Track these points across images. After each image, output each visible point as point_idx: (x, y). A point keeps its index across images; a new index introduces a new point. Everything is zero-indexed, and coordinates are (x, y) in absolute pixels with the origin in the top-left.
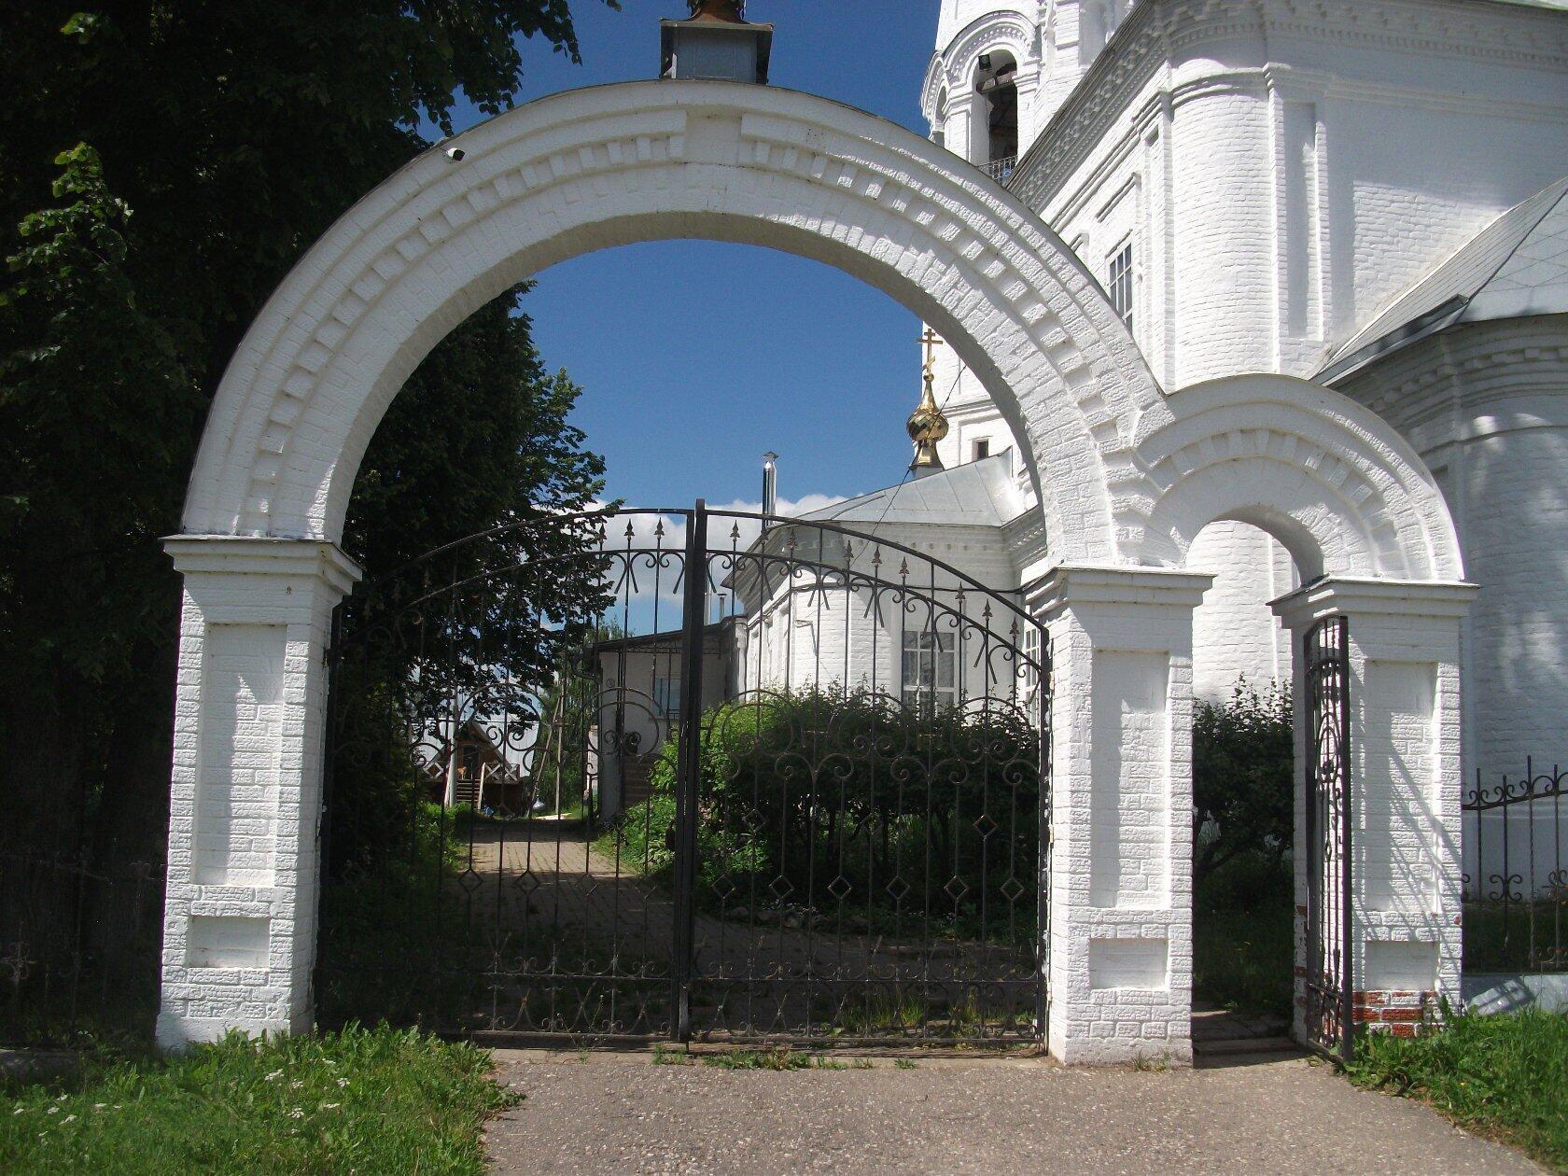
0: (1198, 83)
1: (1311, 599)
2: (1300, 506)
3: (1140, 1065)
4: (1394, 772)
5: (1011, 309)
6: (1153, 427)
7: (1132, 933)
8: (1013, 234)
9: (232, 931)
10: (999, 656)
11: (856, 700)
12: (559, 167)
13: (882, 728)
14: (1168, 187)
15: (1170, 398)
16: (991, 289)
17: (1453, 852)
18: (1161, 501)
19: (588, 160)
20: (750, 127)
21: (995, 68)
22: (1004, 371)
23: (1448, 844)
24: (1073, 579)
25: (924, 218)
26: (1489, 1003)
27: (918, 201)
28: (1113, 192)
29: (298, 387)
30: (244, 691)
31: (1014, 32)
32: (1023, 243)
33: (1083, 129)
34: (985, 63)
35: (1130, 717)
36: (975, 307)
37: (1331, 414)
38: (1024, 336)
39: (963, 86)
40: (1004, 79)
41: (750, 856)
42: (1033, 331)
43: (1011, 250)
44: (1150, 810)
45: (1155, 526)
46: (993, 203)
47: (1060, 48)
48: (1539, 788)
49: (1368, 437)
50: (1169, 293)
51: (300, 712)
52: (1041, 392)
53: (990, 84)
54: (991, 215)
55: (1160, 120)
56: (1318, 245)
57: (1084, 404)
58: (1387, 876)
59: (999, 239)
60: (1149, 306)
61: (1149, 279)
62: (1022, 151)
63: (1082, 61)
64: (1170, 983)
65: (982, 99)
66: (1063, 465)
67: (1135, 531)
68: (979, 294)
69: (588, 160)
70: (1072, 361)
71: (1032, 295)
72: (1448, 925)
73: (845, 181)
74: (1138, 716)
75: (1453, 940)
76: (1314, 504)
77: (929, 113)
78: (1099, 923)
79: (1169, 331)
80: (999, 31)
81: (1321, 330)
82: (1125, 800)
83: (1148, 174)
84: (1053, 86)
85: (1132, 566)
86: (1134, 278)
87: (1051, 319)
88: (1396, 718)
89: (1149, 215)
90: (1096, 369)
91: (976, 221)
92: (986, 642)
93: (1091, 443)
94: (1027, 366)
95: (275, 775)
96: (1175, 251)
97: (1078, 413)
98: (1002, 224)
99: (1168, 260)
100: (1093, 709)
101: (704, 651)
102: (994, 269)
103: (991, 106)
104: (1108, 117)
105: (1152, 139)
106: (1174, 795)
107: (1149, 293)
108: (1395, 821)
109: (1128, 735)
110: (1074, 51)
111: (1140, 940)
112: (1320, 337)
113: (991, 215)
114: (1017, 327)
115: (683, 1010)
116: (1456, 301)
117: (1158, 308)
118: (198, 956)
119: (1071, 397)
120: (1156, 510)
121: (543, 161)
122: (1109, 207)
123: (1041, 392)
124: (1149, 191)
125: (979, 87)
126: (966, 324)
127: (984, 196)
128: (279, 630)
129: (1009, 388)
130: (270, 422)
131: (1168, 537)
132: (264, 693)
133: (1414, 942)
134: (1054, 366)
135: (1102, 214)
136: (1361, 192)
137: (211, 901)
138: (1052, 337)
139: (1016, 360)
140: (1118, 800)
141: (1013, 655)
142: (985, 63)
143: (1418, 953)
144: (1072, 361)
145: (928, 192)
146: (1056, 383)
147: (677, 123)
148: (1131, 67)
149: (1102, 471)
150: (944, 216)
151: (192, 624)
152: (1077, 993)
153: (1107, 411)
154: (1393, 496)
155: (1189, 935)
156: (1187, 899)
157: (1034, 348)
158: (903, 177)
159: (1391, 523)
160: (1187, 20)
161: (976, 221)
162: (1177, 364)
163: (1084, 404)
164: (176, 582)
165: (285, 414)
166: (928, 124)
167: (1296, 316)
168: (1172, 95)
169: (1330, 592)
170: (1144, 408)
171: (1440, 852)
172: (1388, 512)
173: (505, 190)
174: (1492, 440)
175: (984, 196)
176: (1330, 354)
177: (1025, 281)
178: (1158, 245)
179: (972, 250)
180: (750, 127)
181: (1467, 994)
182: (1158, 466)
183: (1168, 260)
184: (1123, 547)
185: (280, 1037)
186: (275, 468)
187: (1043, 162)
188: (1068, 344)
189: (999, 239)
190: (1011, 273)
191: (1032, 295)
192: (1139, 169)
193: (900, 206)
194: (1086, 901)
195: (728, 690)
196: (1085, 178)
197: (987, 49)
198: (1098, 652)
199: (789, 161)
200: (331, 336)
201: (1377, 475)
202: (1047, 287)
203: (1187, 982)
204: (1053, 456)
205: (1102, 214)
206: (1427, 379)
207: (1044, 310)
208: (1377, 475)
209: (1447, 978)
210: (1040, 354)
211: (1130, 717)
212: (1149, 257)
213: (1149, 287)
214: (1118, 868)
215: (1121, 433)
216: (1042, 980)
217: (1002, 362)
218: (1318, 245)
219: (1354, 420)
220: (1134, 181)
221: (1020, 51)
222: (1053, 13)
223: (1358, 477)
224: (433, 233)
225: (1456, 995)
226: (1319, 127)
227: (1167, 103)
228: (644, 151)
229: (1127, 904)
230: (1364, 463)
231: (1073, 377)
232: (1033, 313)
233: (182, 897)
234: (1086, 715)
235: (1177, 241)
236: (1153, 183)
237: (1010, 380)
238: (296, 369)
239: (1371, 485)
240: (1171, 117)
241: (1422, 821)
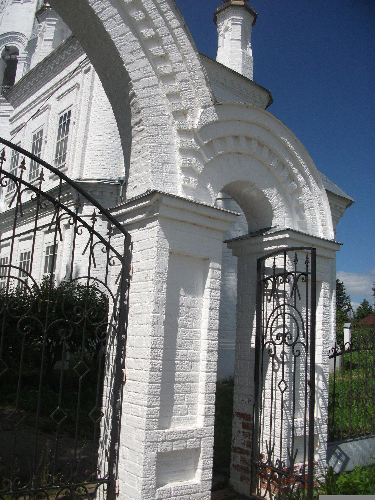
1: (265, 239)
2: (267, 187)
10: (99, 248)
17: (326, 384)
21: (11, 52)
22: (126, 62)
23: (324, 380)
24: (165, 201)
28: (66, 89)
31: (20, 41)
33: (55, 65)
34: (7, 49)
36: (112, 17)
37: (286, 140)
38: (138, 45)
40: (13, 57)
44: (192, 361)
47: (45, 40)
49: (299, 157)
50: (86, 131)
52: (145, 82)
53: (8, 57)
60: (76, 134)
61: (78, 124)
62: (15, 83)
65: (3, 62)
66: (154, 130)
68: (115, 11)
70: (166, 68)
71: (148, 21)
72: (323, 424)
74: (189, 298)
76: (272, 188)
78: (163, 441)
79: (85, 144)
80: (15, 39)
82: (180, 353)
83: (83, 84)
84: (41, 53)
86: (71, 123)
87: (157, 39)
89: (81, 99)
90: (180, 76)
92: (91, 239)
93: (171, 122)
96: (91, 114)
97: (165, 101)
99: (88, 117)
100: (167, 292)
104: (67, 63)
106: (209, 351)
107: (77, 129)
109: (183, 310)
110: (51, 43)
111: (186, 450)
114: (135, 39)
120: (204, 170)
122: (63, 95)
123: (145, 82)
124: (82, 90)
126: (106, 24)
129: (127, 73)
131: (206, 188)
134: (154, 69)
135: (59, 98)
138: (156, 50)
139: (133, 58)
140: (175, 355)
141: (108, 251)
142: (7, 49)
144: (166, 68)
146: (154, 79)
148: (75, 49)
149: (177, 141)
153: (182, 104)
154: (306, 190)
155: (212, 444)
156: (212, 420)
157: (143, 55)
159: (303, 205)
162: (86, 158)
163: (171, 96)
169: (286, 235)
170: (204, 107)
172: (302, 199)
177: (145, 11)
178: (83, 111)
182: (207, 144)
183: (88, 117)
184: (185, 188)
187: (35, 77)
191: (148, 21)
192: (80, 82)
194: (156, 426)
196: (53, 84)
197: (9, 44)
201: (300, 178)
203: (210, 475)
204: (150, 123)
207: (153, 33)
208: (300, 178)
210: (147, 60)
211: (185, 299)
212: (79, 116)
213: (77, 127)
214: (173, 400)
215: (189, 119)
219: (294, 147)
220: (77, 86)
221: (21, 48)
222: (45, 27)
223: (292, 178)
229: (177, 427)
230: (295, 171)
232: (148, 33)
235: (92, 110)
237: (128, 68)
239: (297, 183)
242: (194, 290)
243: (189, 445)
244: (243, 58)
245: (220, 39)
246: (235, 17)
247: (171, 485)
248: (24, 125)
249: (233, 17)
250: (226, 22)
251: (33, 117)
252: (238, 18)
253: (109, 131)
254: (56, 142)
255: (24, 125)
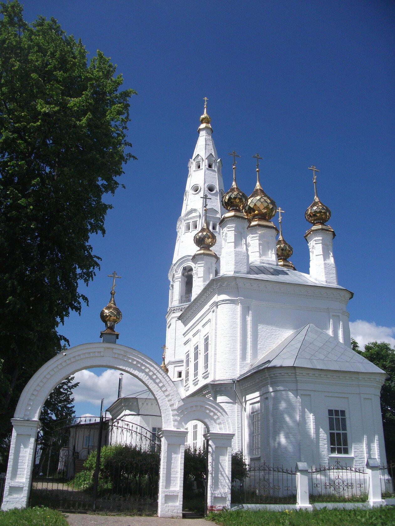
0: (223, 301)
3: (173, 518)
4: (220, 466)
5: (157, 384)
6: (180, 405)
7: (172, 494)
8: (158, 371)
9: (15, 489)
11: (135, 448)
12: (82, 357)
13: (142, 455)
14: (216, 324)
15: (183, 400)
16: (154, 380)
18: (181, 418)
19: (87, 355)
20: (114, 351)
21: (187, 270)
23: (229, 479)
25: (143, 368)
26: (235, 508)
27: (142, 365)
29: (35, 393)
30: (22, 446)
32: (159, 373)
34: (185, 269)
35: (174, 456)
39: (179, 274)
40: (190, 273)
41: (109, 486)
42: (161, 388)
43: (157, 374)
45: (180, 422)
46: (155, 366)
48: (252, 469)
51: (32, 451)
54: (154, 368)
55: (215, 308)
56: (249, 340)
57: (169, 401)
58: (218, 485)
59: (155, 372)
63: (204, 281)
64: (179, 503)
67: (176, 423)
69: (87, 355)
70: (167, 393)
71: (161, 381)
73: (130, 361)
75: (229, 497)
77: (170, 279)
81: (249, 360)
82: (172, 470)
85: (175, 429)
87: (164, 386)
88: (220, 457)
91: (152, 368)
94: (159, 394)
95: (27, 461)
98: (156, 369)
101: (103, 428)
102: (154, 377)
103: (186, 279)
105: (213, 311)
108: (220, 475)
110: (202, 279)
111: (173, 495)
112: (249, 362)
113: (154, 368)
115: (94, 506)
116: (269, 362)
117: (213, 353)
118: (10, 493)
119: (167, 399)
121: (79, 355)
125: (183, 274)
127: (153, 364)
128: (29, 436)
130: (30, 399)
132: (26, 446)
133: (222, 497)
136: (260, 327)
137: (14, 484)
138: (164, 389)
143: (223, 499)
144: (167, 393)
145: (144, 363)
146: (164, 397)
147: (102, 350)
149: (171, 412)
150: (146, 367)
151: (14, 433)
152: (162, 504)
156: (182, 488)
158: (140, 361)
160: (221, 286)
161: (152, 368)
163: (169, 401)
164: (12, 426)
165: (32, 398)
166: (170, 282)
167: (244, 357)
168: (217, 303)
171: (227, 481)
173: (72, 360)
174: (272, 393)
175: (153, 364)
176: (251, 365)
179: (151, 373)
180: (114, 351)
181: (231, 507)
184: (174, 426)
185: (24, 508)
186: (30, 407)
188: (166, 390)
189: (155, 372)
190: (157, 378)
191: (161, 381)
193: (139, 365)
195: (106, 442)
197: (185, 265)
198: (169, 444)
199: (121, 357)
200: (41, 384)
202: (163, 380)
203: (182, 503)
205: (204, 326)
206: (264, 377)
209: (228, 504)
211: (174, 456)
216: (157, 503)
217: (155, 393)
218: (249, 340)
220: (209, 321)
224: (60, 367)
225: (230, 507)
226: (250, 312)
227: (216, 304)
228: (97, 354)
229: (172, 489)
231: (167, 396)
232: (161, 385)
233: (9, 483)
234: (166, 455)
236: (213, 322)
238: (35, 390)
240: (217, 307)
241: (224, 475)
242: (373, 442)
243: (175, 494)
244: (325, 268)
245: (311, 254)
246: (316, 238)
247: (170, 504)
248: (198, 331)
249: (315, 239)
250: (312, 242)
251: (194, 335)
252: (319, 238)
253: (227, 349)
254: (209, 352)
255: (198, 331)
